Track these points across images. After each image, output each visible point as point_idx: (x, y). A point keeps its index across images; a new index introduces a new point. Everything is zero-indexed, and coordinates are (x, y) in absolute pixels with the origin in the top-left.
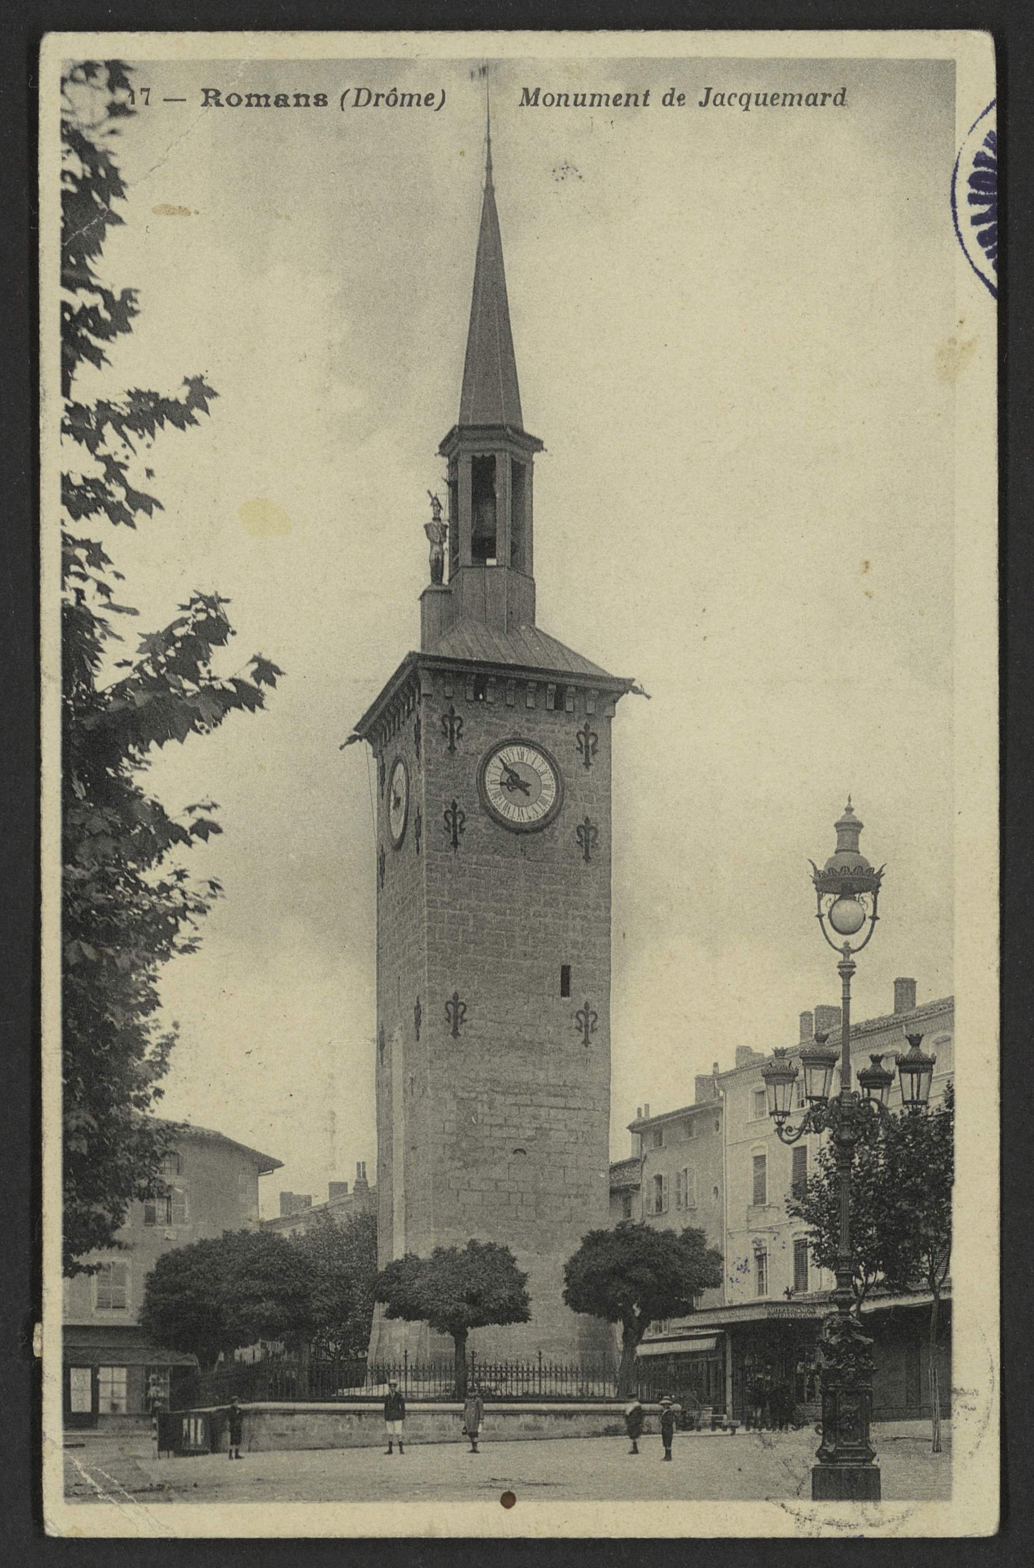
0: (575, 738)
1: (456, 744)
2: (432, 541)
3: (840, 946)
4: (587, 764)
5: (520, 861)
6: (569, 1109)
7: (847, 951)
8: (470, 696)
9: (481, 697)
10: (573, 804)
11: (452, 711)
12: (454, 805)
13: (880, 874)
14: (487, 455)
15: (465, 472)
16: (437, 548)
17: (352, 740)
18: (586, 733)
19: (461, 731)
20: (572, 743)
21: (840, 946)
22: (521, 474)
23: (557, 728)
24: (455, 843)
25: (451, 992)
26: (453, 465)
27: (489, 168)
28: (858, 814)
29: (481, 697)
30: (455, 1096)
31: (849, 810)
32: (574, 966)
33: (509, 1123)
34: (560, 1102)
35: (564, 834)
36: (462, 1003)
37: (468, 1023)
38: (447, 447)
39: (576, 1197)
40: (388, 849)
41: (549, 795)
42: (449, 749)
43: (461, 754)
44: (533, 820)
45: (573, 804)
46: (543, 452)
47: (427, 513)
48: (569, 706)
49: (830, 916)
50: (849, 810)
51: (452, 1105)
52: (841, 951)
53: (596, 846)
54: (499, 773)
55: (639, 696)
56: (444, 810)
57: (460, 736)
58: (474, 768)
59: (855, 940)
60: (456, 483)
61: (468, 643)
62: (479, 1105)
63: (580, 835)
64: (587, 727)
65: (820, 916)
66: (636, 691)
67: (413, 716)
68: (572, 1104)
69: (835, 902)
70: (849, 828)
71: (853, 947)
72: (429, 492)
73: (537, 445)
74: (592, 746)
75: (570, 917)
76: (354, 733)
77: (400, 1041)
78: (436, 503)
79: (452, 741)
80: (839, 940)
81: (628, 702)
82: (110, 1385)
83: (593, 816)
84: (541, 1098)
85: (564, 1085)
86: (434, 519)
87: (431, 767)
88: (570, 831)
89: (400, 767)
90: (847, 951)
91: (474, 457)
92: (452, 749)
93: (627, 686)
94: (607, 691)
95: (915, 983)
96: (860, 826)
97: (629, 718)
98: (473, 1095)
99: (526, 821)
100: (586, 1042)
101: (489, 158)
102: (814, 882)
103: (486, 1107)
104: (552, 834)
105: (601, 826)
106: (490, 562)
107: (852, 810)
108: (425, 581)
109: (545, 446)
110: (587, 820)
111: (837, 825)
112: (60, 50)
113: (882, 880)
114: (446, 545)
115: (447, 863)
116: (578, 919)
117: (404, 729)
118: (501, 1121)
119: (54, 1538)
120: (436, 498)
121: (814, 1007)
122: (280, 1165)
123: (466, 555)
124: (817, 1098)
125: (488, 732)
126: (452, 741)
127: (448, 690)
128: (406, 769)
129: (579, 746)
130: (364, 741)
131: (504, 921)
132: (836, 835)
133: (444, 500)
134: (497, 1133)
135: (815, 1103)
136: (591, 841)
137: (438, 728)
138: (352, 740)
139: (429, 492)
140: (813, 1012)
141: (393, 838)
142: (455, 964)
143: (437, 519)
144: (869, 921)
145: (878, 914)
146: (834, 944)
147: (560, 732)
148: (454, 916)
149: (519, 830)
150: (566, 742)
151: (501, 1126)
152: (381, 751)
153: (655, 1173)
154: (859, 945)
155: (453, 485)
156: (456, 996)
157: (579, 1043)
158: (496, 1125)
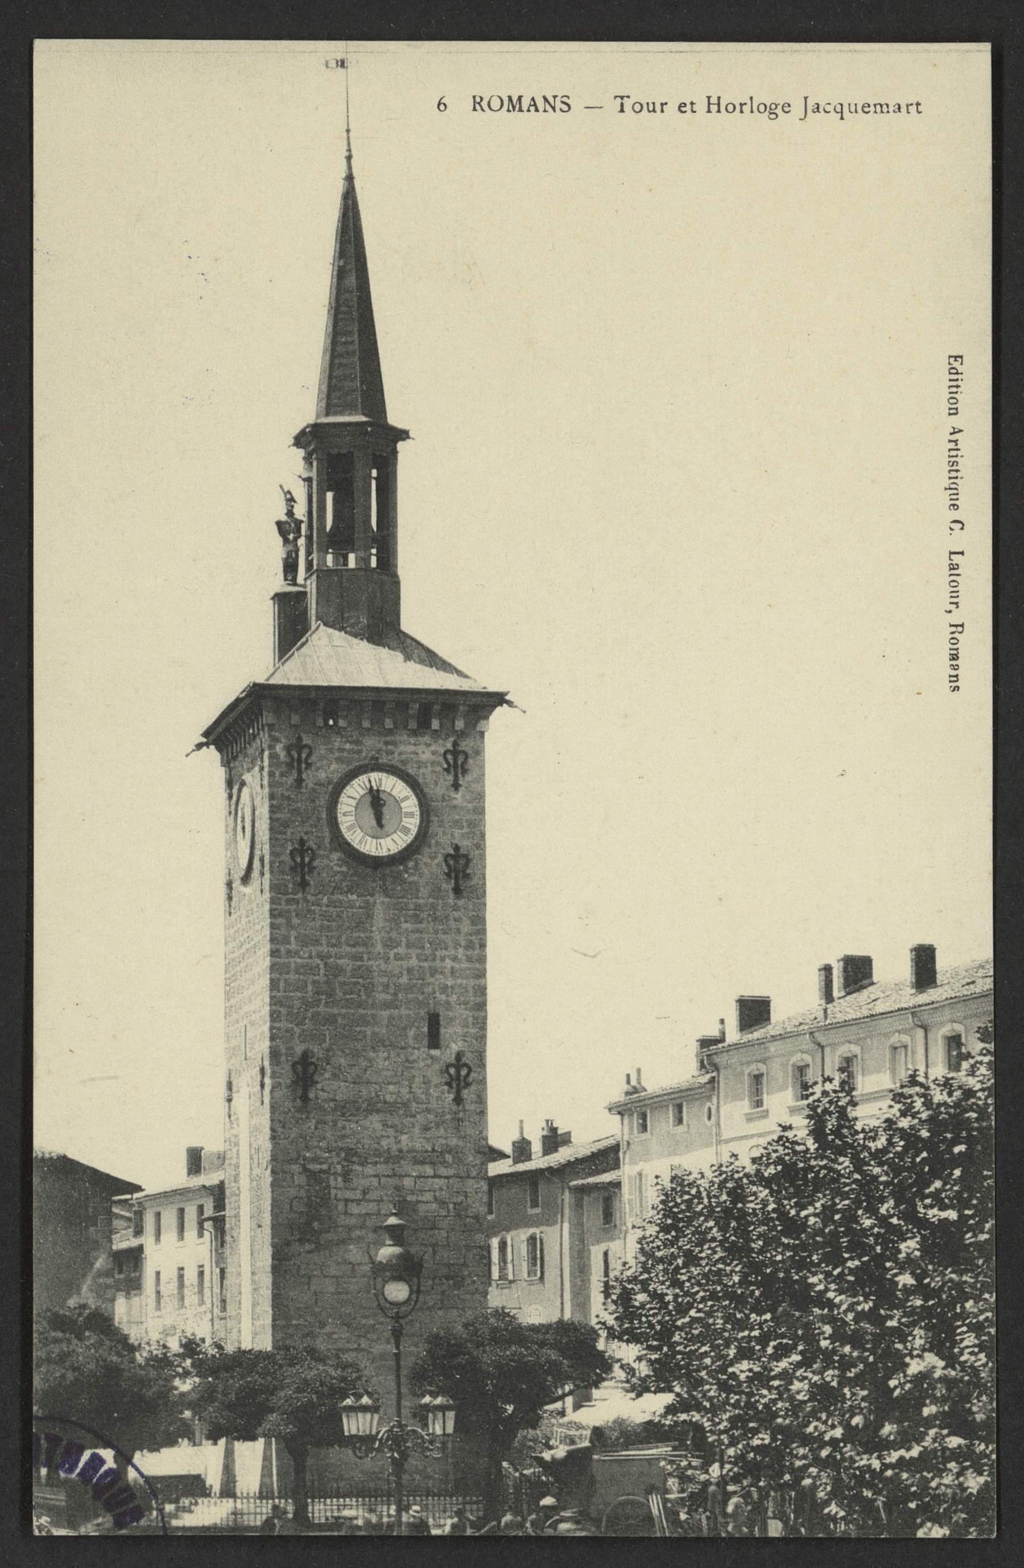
0: (441, 759)
1: (304, 776)
4: (456, 786)
6: (440, 1177)
8: (320, 722)
9: (331, 722)
10: (440, 831)
11: (300, 739)
12: (302, 842)
16: (291, 547)
17: (199, 746)
18: (455, 752)
20: (439, 764)
22: (387, 465)
23: (420, 749)
24: (304, 885)
25: (299, 1049)
27: (349, 158)
29: (331, 722)
30: (305, 1170)
34: (429, 1170)
35: (431, 865)
36: (312, 1063)
37: (319, 1086)
39: (447, 1278)
41: (413, 824)
42: (296, 780)
43: (311, 785)
44: (392, 852)
45: (440, 831)
46: (408, 441)
48: (435, 724)
51: (301, 1180)
54: (362, 792)
56: (290, 848)
57: (309, 765)
58: (323, 801)
63: (448, 865)
64: (455, 744)
66: (510, 703)
72: (281, 487)
74: (461, 764)
75: (438, 957)
78: (291, 500)
79: (300, 772)
81: (500, 713)
83: (465, 844)
84: (406, 1167)
85: (433, 1150)
87: (275, 802)
88: (436, 861)
91: (329, 454)
92: (299, 781)
99: (385, 854)
101: (349, 144)
103: (340, 1179)
104: (416, 867)
110: (457, 848)
112: (36, 1533)
115: (294, 907)
116: (447, 961)
118: (358, 1195)
119: (566, 1457)
125: (339, 760)
126: (300, 772)
127: (295, 719)
129: (445, 766)
131: (360, 967)
134: (355, 1209)
139: (281, 487)
147: (425, 752)
148: (303, 966)
149: (376, 863)
150: (433, 763)
151: (358, 1202)
158: (352, 1201)
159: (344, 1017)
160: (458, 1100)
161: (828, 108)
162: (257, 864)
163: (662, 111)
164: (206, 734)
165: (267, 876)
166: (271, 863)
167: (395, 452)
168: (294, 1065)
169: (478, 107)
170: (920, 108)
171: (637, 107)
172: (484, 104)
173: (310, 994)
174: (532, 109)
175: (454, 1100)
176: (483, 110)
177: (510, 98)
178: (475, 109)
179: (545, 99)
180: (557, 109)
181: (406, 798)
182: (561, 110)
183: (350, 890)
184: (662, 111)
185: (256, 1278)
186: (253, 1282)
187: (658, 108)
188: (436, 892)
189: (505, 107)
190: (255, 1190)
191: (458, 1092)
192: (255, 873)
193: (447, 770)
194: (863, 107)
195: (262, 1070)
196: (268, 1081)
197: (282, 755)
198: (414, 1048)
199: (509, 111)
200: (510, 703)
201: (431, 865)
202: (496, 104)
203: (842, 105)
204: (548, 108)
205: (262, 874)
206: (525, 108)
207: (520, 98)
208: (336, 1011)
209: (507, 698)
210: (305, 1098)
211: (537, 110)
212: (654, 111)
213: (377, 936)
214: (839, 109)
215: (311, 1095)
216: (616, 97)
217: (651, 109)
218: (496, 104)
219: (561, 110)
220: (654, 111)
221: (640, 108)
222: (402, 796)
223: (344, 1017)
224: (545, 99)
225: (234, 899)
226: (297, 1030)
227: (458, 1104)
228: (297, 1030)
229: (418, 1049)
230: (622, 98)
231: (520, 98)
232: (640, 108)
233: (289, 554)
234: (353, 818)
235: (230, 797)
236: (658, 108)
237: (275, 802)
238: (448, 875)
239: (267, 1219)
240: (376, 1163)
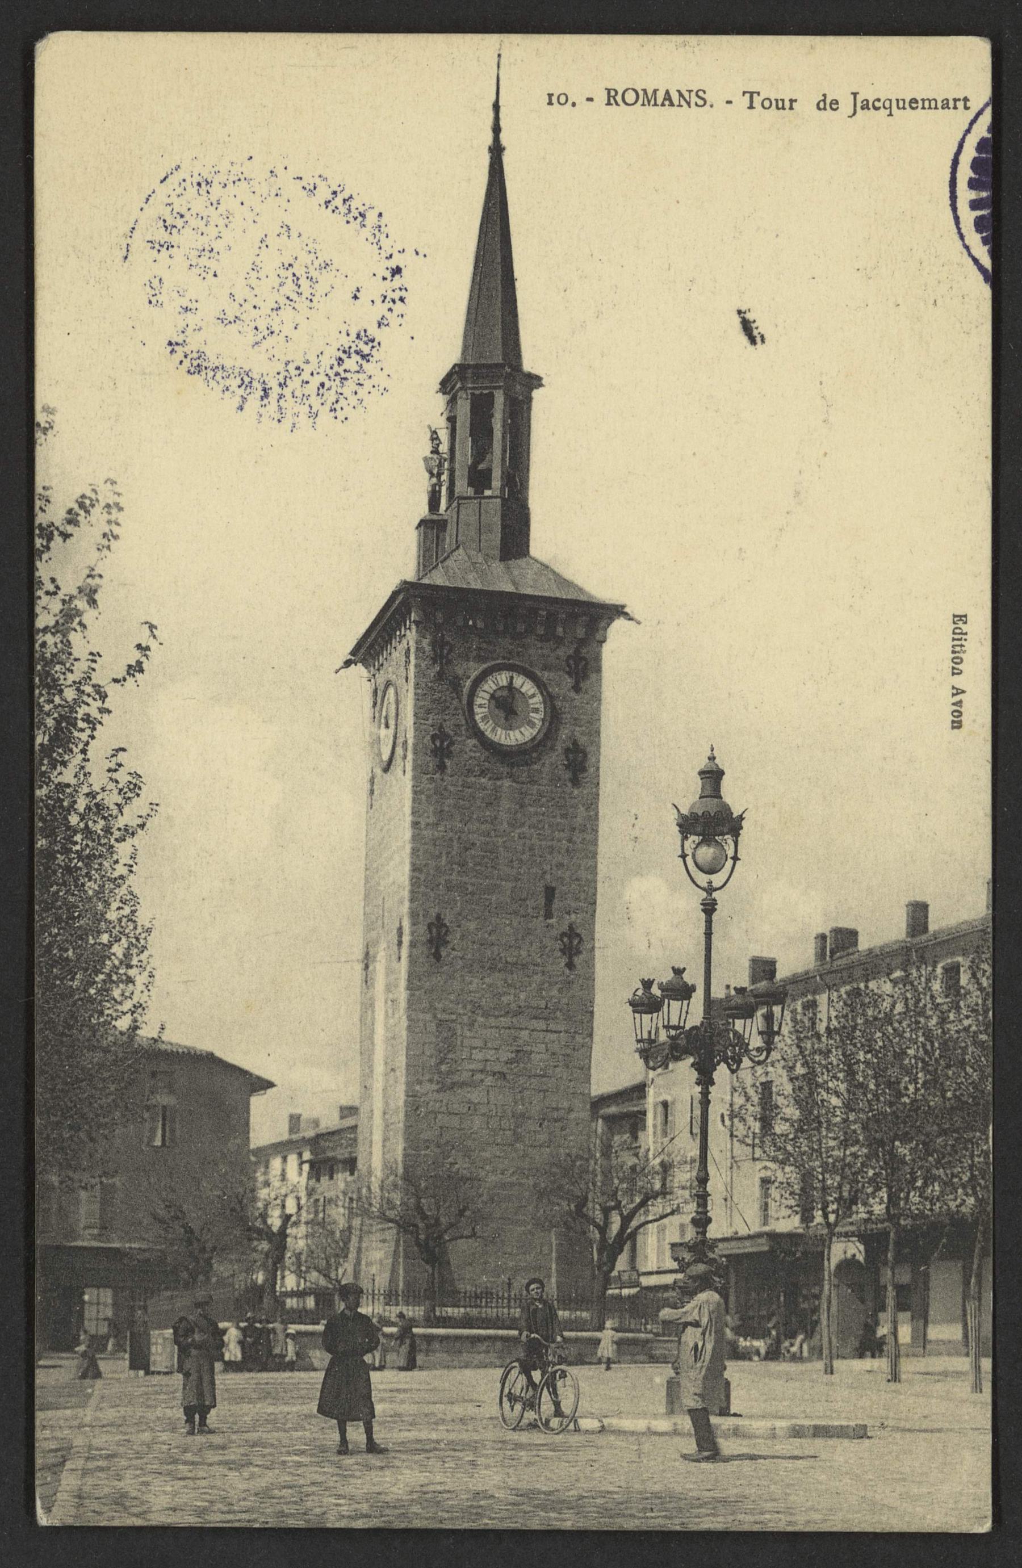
2: (432, 474)
3: (705, 885)
5: (507, 783)
6: (551, 1031)
7: (710, 889)
13: (741, 818)
14: (486, 392)
15: (464, 408)
16: (434, 480)
17: (348, 664)
19: (450, 657)
21: (705, 885)
25: (433, 912)
26: (452, 402)
28: (721, 762)
30: (435, 1017)
31: (712, 758)
32: (560, 889)
33: (489, 1045)
34: (541, 1025)
38: (446, 385)
40: (378, 771)
47: (425, 448)
49: (694, 856)
50: (712, 758)
52: (704, 889)
53: (584, 770)
55: (631, 622)
59: (717, 879)
60: (455, 417)
61: (458, 572)
62: (459, 1026)
65: (683, 856)
67: (404, 641)
68: (552, 1027)
69: (699, 844)
70: (712, 777)
71: (715, 885)
73: (534, 381)
74: (584, 668)
76: (349, 657)
77: (384, 961)
78: (434, 437)
80: (702, 879)
81: (619, 625)
82: (95, 1307)
83: (583, 740)
86: (432, 452)
87: (419, 691)
89: (391, 691)
90: (710, 889)
93: (618, 611)
94: (593, 617)
95: (927, 906)
96: (722, 773)
97: (618, 645)
98: (454, 1017)
99: (513, 743)
100: (570, 965)
102: (678, 825)
105: (591, 749)
106: (488, 493)
107: (714, 758)
108: (422, 510)
109: (544, 382)
110: (575, 743)
111: (701, 773)
113: (744, 823)
114: (444, 477)
117: (395, 655)
120: (435, 432)
121: (829, 928)
122: (270, 1085)
123: (462, 487)
124: (674, 1028)
128: (397, 693)
130: (360, 665)
132: (700, 782)
133: (444, 435)
135: (673, 1032)
136: (580, 764)
137: (427, 654)
138: (348, 664)
140: (828, 934)
141: (382, 761)
142: (438, 885)
143: (435, 451)
144: (729, 863)
145: (681, 859)
146: (698, 883)
152: (374, 675)
153: (661, 1099)
154: (721, 884)
155: (452, 420)
156: (438, 917)
157: (563, 964)
159: (473, 885)
160: (570, 965)
161: (877, 104)
162: (399, 751)
163: (791, 108)
164: (353, 653)
165: (410, 756)
166: (415, 745)
167: (529, 399)
168: (430, 926)
169: (612, 101)
170: (968, 104)
171: (767, 104)
172: (619, 98)
173: (443, 863)
174: (667, 103)
175: (566, 965)
176: (617, 104)
177: (645, 91)
178: (609, 104)
179: (681, 95)
180: (693, 104)
181: (533, 696)
182: (696, 105)
183: (483, 773)
184: (791, 108)
185: (387, 1117)
186: (385, 1120)
187: (787, 104)
188: (555, 779)
189: (640, 102)
190: (391, 1039)
191: (570, 958)
192: (398, 760)
193: (569, 674)
194: (911, 102)
195: (400, 931)
196: (406, 939)
197: (428, 648)
198: (533, 917)
199: (643, 105)
200: (626, 615)
201: (555, 758)
202: (630, 97)
203: (890, 100)
204: (683, 102)
205: (405, 757)
206: (659, 101)
207: (655, 91)
208: (465, 879)
209: (626, 610)
210: (437, 956)
211: (672, 104)
212: (783, 108)
213: (503, 816)
214: (887, 105)
215: (443, 954)
216: (744, 93)
217: (780, 106)
218: (630, 97)
219: (696, 105)
220: (783, 108)
221: (769, 104)
222: (530, 693)
223: (473, 885)
224: (681, 95)
225: (376, 793)
226: (432, 894)
227: (570, 969)
228: (432, 894)
229: (537, 917)
230: (752, 94)
231: (655, 91)
232: (769, 104)
233: (434, 486)
234: (486, 710)
235: (375, 704)
236: (787, 104)
237: (419, 691)
238: (567, 767)
239: (402, 1060)
240: (497, 1017)
